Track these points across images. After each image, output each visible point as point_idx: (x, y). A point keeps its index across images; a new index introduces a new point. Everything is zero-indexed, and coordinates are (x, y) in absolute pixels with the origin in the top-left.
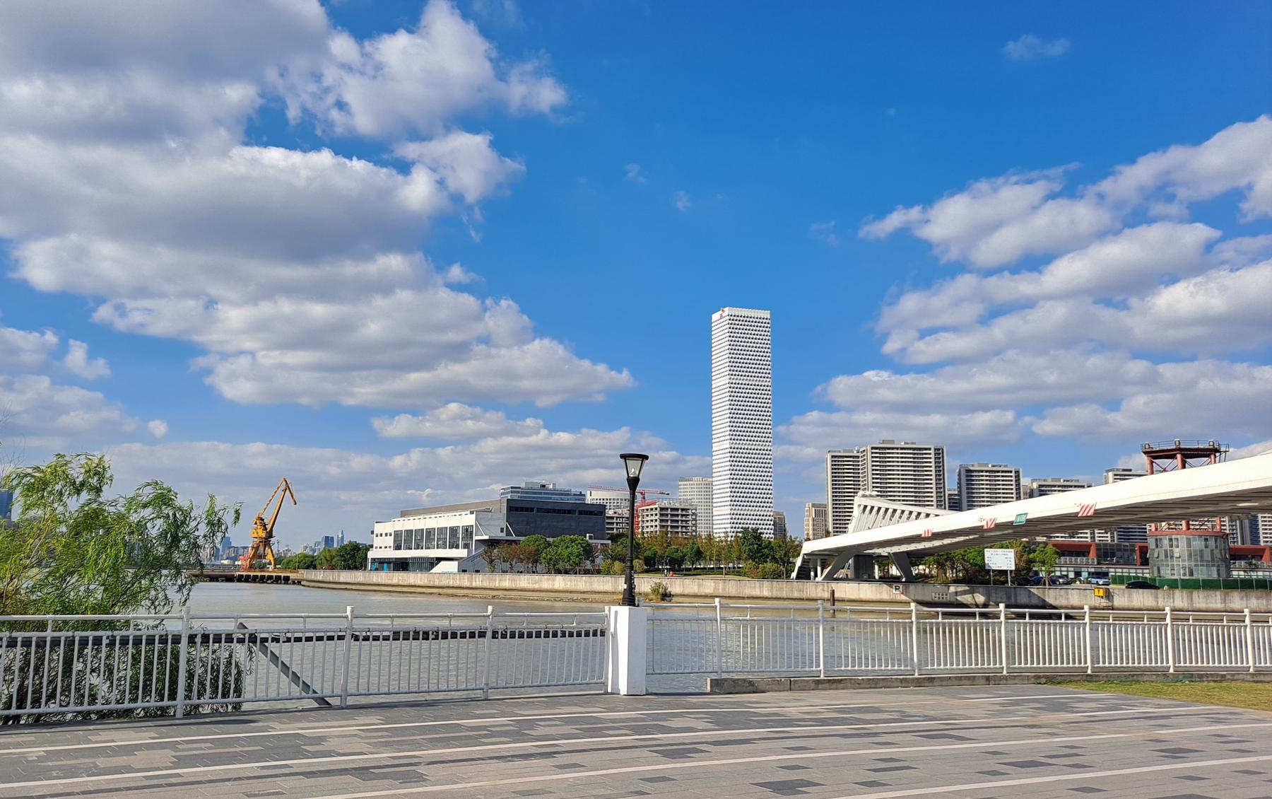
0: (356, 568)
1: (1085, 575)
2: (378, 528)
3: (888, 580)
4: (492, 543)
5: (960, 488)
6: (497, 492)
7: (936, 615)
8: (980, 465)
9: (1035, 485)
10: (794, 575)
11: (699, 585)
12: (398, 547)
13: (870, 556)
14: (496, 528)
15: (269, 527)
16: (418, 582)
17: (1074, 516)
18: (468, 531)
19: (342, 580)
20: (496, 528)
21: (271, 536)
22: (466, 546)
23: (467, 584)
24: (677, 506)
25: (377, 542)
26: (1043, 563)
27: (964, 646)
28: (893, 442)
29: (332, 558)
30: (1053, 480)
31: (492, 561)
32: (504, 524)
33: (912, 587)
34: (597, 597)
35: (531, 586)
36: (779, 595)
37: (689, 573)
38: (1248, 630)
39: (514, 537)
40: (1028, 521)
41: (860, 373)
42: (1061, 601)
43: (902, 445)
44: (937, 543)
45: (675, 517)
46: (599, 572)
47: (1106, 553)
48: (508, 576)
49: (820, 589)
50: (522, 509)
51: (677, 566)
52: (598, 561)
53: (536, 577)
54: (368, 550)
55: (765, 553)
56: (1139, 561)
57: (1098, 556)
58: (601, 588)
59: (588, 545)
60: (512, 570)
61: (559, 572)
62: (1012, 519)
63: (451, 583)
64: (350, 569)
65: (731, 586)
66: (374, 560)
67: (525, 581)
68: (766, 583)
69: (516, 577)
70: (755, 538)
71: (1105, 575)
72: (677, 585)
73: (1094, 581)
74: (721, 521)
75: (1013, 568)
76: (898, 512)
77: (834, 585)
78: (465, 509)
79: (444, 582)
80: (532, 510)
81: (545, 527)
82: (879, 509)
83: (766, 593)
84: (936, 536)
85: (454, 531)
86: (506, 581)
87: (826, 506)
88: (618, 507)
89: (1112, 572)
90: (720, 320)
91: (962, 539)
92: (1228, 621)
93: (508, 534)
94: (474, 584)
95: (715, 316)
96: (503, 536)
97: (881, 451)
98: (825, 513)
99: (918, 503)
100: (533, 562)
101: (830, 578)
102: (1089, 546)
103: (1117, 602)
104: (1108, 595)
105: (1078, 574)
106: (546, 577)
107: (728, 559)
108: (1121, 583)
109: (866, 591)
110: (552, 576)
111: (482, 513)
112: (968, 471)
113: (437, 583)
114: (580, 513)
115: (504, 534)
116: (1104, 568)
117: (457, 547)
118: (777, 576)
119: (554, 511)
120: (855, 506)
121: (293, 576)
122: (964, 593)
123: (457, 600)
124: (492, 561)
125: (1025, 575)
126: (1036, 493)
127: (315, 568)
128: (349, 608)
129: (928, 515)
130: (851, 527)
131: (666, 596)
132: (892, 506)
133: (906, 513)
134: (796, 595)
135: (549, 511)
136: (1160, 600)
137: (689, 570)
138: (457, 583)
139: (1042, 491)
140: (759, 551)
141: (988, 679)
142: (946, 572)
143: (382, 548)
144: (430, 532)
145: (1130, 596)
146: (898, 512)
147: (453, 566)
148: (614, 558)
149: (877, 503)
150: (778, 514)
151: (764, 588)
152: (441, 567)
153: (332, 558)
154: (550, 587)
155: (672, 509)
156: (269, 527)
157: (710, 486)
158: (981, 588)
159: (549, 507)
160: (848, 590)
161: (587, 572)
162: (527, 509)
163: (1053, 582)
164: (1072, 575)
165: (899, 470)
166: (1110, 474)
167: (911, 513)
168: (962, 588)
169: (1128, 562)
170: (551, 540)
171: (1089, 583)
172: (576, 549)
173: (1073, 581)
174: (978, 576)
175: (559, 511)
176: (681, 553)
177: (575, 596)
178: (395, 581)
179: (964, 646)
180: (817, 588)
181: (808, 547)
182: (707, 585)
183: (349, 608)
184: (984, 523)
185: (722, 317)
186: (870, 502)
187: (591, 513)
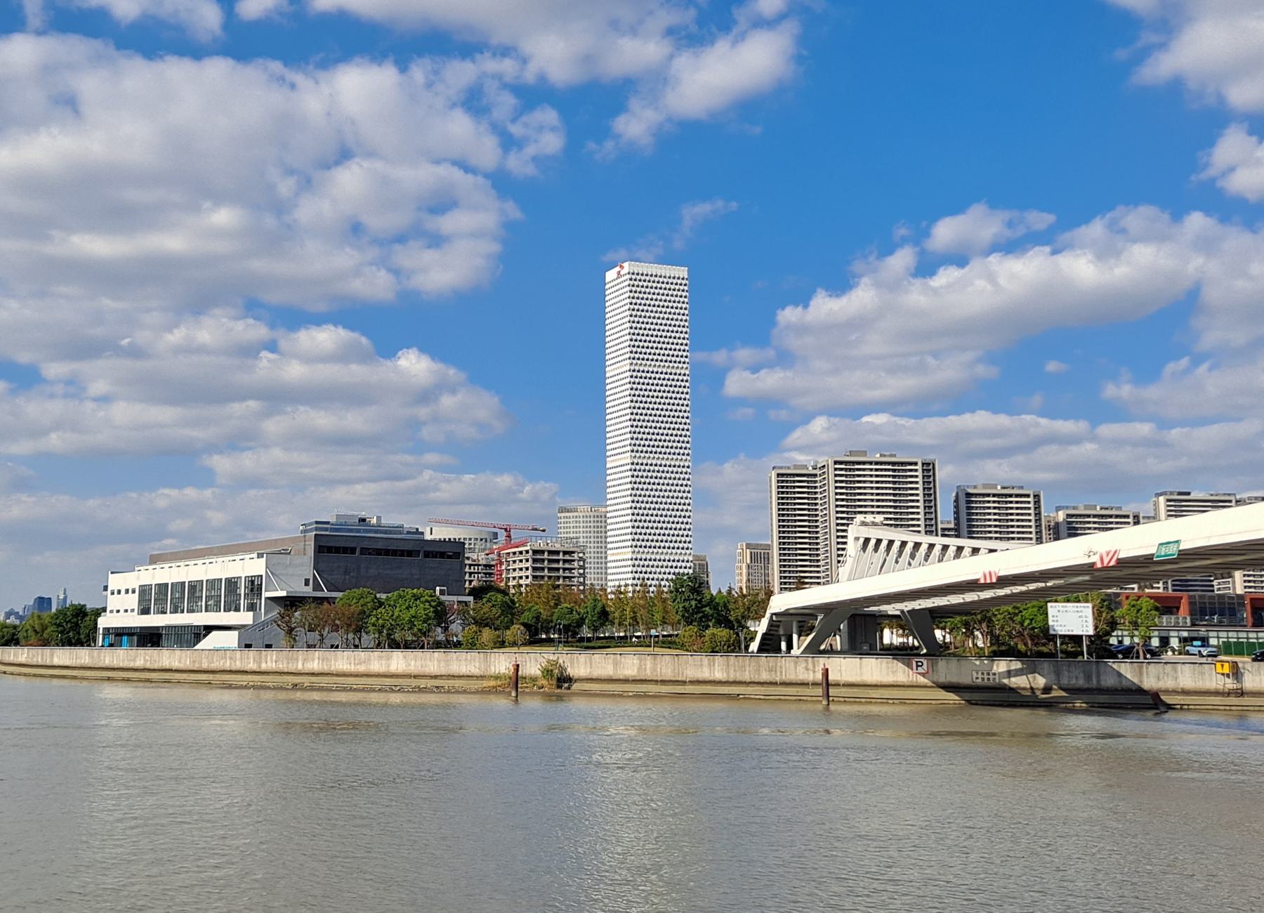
0: (80, 643)
1: (1174, 643)
2: (115, 581)
4: (291, 603)
5: (957, 519)
6: (292, 521)
9: (1061, 516)
10: (754, 646)
11: (616, 664)
12: (145, 611)
13: (873, 616)
14: (298, 578)
16: (176, 665)
17: (1147, 560)
18: (254, 586)
19: (56, 662)
20: (298, 578)
22: (252, 607)
23: (252, 666)
24: (558, 547)
25: (113, 602)
28: (864, 453)
29: (44, 628)
30: (1086, 507)
31: (291, 630)
32: (309, 572)
33: (942, 663)
34: (458, 683)
36: (739, 678)
39: (326, 593)
40: (1119, 561)
42: (1167, 683)
43: (877, 457)
45: (555, 564)
46: (458, 645)
48: (317, 654)
50: (337, 550)
52: (455, 627)
53: (361, 654)
54: (98, 615)
55: (703, 614)
56: (1250, 620)
59: (441, 603)
60: (321, 643)
61: (395, 645)
62: (1152, 550)
63: (227, 665)
64: (70, 644)
65: (663, 665)
66: (107, 631)
67: (344, 661)
68: (719, 660)
69: (331, 654)
72: (580, 664)
74: (618, 569)
76: (924, 548)
77: (822, 661)
78: (251, 551)
81: (371, 580)
82: (879, 541)
83: (719, 675)
84: (1003, 581)
85: (232, 584)
86: (315, 661)
87: (769, 547)
90: (617, 282)
93: (317, 587)
94: (264, 667)
95: (611, 275)
96: (308, 591)
97: (847, 467)
98: (767, 558)
100: (357, 628)
104: (1236, 673)
105: (1165, 641)
106: (377, 654)
109: (873, 669)
110: (387, 653)
111: (276, 553)
112: (969, 495)
113: (205, 666)
114: (427, 555)
116: (1202, 632)
117: (237, 609)
120: (850, 540)
122: (1018, 673)
124: (291, 630)
126: (1063, 530)
127: (17, 643)
129: (975, 551)
130: (844, 571)
131: (564, 680)
132: (911, 538)
134: (765, 677)
135: (378, 552)
137: (589, 640)
138: (238, 665)
139: (1071, 529)
140: (698, 610)
143: (121, 612)
144: (194, 587)
147: (231, 639)
148: (482, 623)
149: (886, 534)
150: (697, 558)
151: (715, 668)
153: (44, 628)
155: (550, 552)
158: (1046, 665)
159: (380, 546)
160: (847, 669)
161: (437, 645)
162: (345, 550)
166: (1162, 499)
168: (1016, 665)
170: (384, 596)
172: (422, 610)
174: (1041, 646)
175: (394, 553)
176: (564, 614)
177: (422, 683)
178: (139, 663)
180: (796, 665)
181: (782, 602)
182: (629, 663)
186: (874, 533)
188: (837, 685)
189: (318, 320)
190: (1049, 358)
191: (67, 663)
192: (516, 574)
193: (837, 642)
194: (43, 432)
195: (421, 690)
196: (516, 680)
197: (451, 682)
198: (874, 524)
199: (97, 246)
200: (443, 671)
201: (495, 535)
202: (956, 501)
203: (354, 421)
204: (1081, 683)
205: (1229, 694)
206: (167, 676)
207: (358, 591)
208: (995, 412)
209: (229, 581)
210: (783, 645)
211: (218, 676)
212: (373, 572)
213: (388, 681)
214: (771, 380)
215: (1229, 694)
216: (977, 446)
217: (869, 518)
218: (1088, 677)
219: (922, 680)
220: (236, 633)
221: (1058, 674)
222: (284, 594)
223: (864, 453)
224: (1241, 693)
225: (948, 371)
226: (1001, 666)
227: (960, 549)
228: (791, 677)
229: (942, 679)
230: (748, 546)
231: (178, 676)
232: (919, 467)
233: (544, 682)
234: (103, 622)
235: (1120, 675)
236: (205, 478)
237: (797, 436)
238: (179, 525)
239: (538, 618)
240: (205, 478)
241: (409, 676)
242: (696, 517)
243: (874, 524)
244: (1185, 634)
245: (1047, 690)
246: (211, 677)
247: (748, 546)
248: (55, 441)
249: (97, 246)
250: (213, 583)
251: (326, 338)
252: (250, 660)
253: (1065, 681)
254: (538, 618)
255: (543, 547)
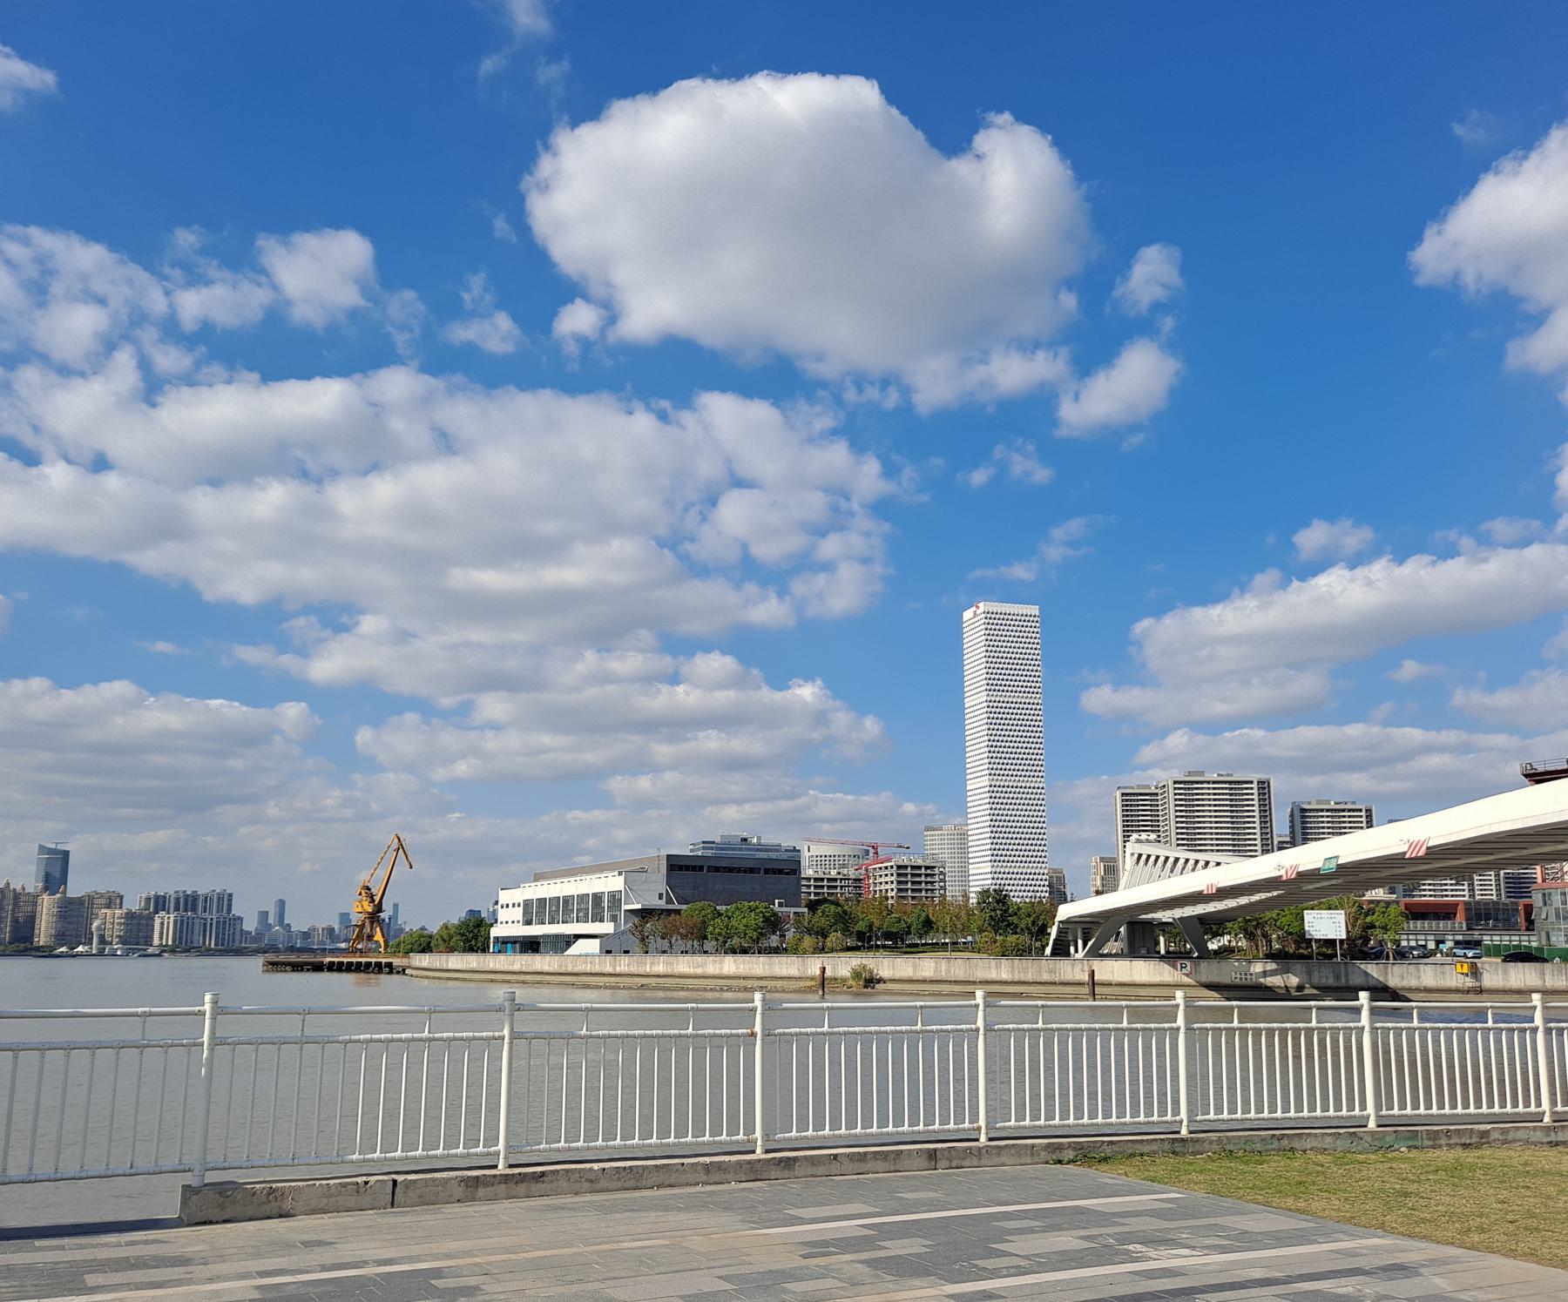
0: (472, 950)
2: (505, 897)
3: (1171, 957)
4: (645, 914)
7: (1226, 1014)
8: (1319, 802)
10: (1048, 950)
11: (915, 966)
12: (528, 923)
13: (1149, 923)
14: (654, 893)
15: (377, 899)
16: (546, 968)
18: (615, 898)
19: (451, 966)
20: (654, 893)
21: (380, 910)
22: (614, 919)
23: (609, 969)
24: (920, 862)
25: (503, 915)
26: (1385, 929)
27: (1297, 1057)
28: (1202, 774)
32: (663, 887)
33: (1204, 964)
34: (779, 984)
35: (692, 971)
36: (1023, 978)
37: (913, 949)
38: (1540, 1036)
39: (676, 906)
40: (1340, 867)
41: (26, 225)
43: (1215, 777)
44: (1231, 903)
45: (917, 878)
47: (1480, 915)
49: (1078, 967)
50: (687, 868)
51: (898, 940)
55: (1013, 924)
57: (1468, 919)
58: (785, 972)
59: (775, 914)
61: (734, 951)
62: (1319, 865)
63: (588, 968)
66: (497, 939)
68: (1005, 962)
70: (998, 902)
71: (1478, 943)
72: (887, 966)
73: (1459, 952)
75: (1344, 937)
76: (1182, 861)
79: (579, 968)
80: (701, 868)
81: (726, 895)
82: (1158, 857)
83: (1005, 976)
85: (597, 898)
86: (659, 965)
88: (844, 866)
89: (1487, 940)
90: (973, 618)
91: (1263, 896)
92: (1421, 1020)
93: (669, 901)
94: (618, 970)
95: (967, 615)
96: (662, 904)
99: (1192, 846)
100: (699, 937)
101: (1095, 953)
102: (1456, 905)
103: (1489, 980)
104: (1475, 972)
107: (965, 930)
108: (1497, 955)
109: (1142, 971)
111: (633, 873)
112: (1303, 810)
113: (570, 969)
114: (767, 871)
115: (663, 902)
116: (1476, 936)
117: (602, 921)
118: (1022, 952)
119: (731, 870)
121: (396, 962)
122: (1273, 973)
123: (473, 985)
125: (1359, 947)
128: (208, 997)
129: (1218, 864)
133: (1192, 862)
134: (1045, 977)
136: (1548, 978)
137: (916, 945)
138: (597, 969)
141: (933, 1156)
142: (1258, 951)
143: (509, 924)
144: (567, 900)
145: (1505, 972)
146: (1182, 861)
149: (1154, 850)
150: (1055, 871)
152: (580, 947)
153: (451, 937)
154: (717, 972)
156: (377, 899)
157: (964, 836)
158: (1299, 966)
162: (694, 868)
163: (1401, 955)
164: (1431, 945)
165: (1210, 805)
167: (1197, 862)
168: (1271, 966)
169: (1508, 925)
171: (1455, 955)
172: (754, 920)
173: (1432, 953)
174: (1300, 951)
175: (739, 870)
178: (517, 967)
179: (1297, 1057)
180: (1074, 968)
181: (1065, 912)
182: (927, 966)
183: (208, 997)
184: (1282, 872)
185: (975, 615)
186: (1146, 849)
187: (781, 872)
188: (1103, 984)
189: (707, 648)
190: (1367, 668)
191: (460, 967)
192: (883, 887)
193: (1112, 946)
194: (453, 760)
195: (939, 995)
196: (823, 981)
197: (774, 983)
198: (1148, 841)
199: (490, 579)
200: (767, 973)
201: (867, 852)
202: (1292, 816)
203: (742, 744)
204: (1331, 982)
205: (1468, 992)
206: (539, 978)
207: (699, 904)
208: (1427, 729)
209: (595, 895)
210: (1072, 949)
211: (580, 978)
212: (718, 887)
213: (721, 982)
214: (1131, 699)
215: (1468, 992)
216: (1291, 760)
217: (1144, 836)
218: (1337, 977)
219: (1186, 980)
220: (597, 941)
221: (1309, 974)
222: (639, 906)
223: (1202, 774)
224: (1480, 991)
225: (1307, 685)
226: (1258, 967)
227: (1207, 863)
228: (1069, 977)
229: (1204, 979)
230: (1102, 860)
231: (548, 978)
232: (1255, 785)
233: (851, 982)
234: (495, 932)
235: (1366, 974)
236: (606, 801)
237: (1148, 753)
238: (591, 843)
239: (871, 926)
240: (606, 801)
241: (739, 978)
242: (1051, 832)
243: (1148, 841)
244: (1460, 938)
245: (1300, 988)
246: (575, 979)
247: (1102, 860)
248: (462, 768)
249: (490, 579)
250: (583, 898)
251: (715, 664)
252: (607, 964)
253: (1315, 981)
254: (871, 926)
255: (906, 863)
